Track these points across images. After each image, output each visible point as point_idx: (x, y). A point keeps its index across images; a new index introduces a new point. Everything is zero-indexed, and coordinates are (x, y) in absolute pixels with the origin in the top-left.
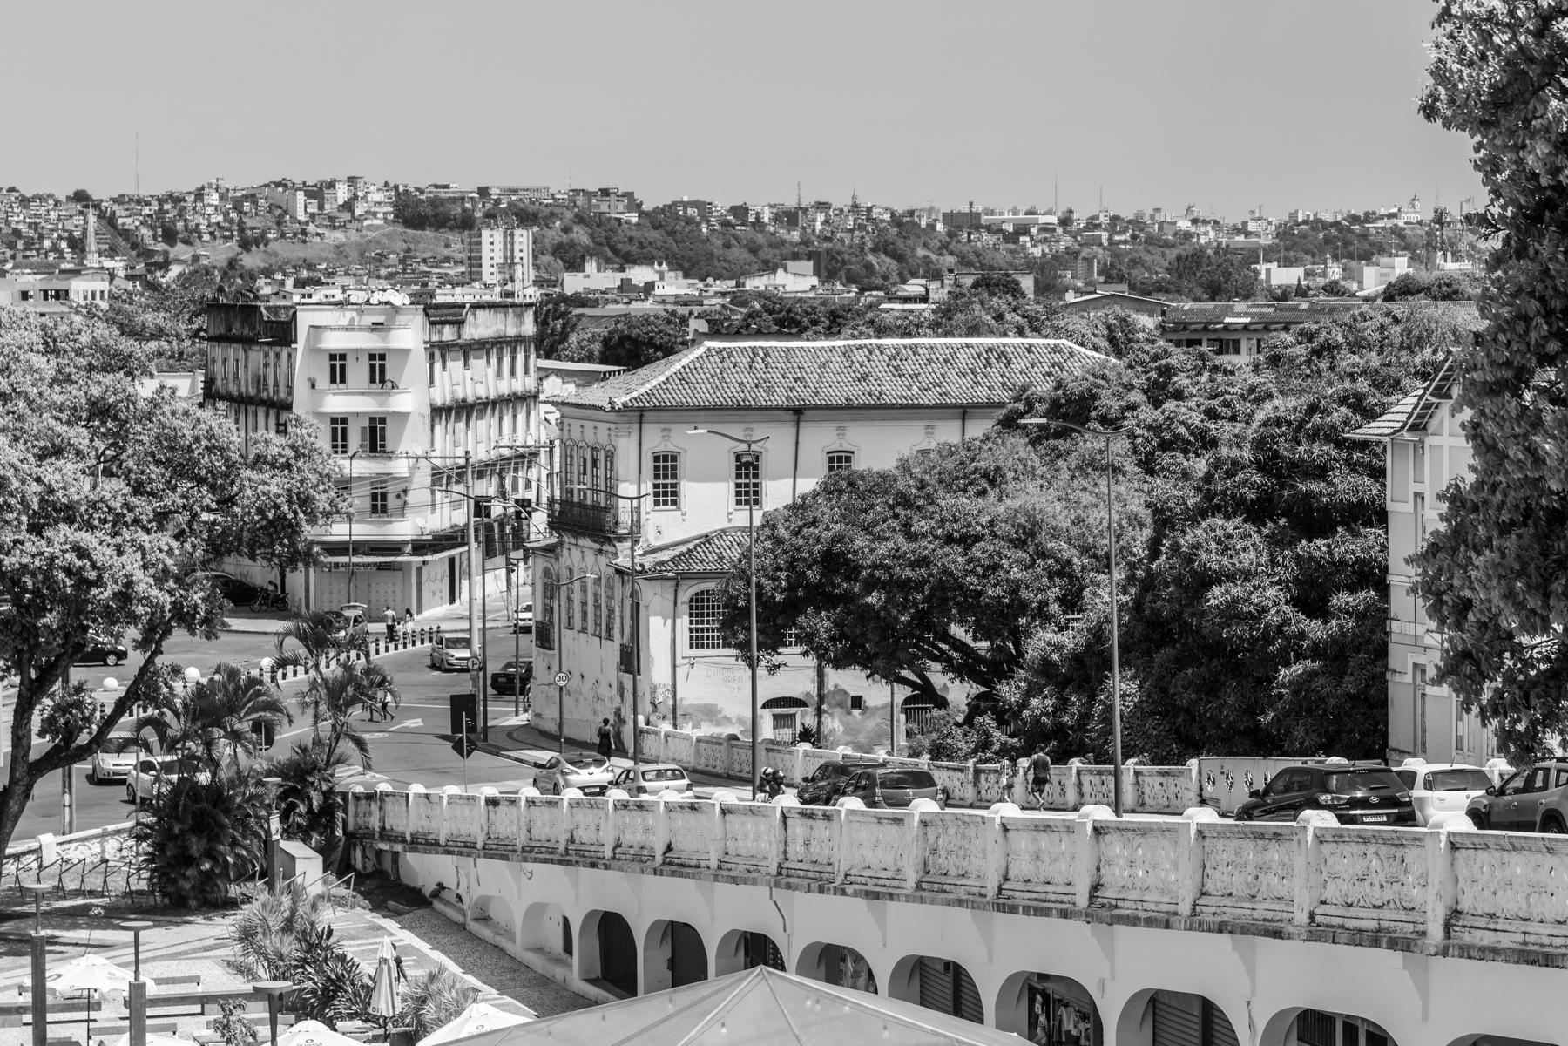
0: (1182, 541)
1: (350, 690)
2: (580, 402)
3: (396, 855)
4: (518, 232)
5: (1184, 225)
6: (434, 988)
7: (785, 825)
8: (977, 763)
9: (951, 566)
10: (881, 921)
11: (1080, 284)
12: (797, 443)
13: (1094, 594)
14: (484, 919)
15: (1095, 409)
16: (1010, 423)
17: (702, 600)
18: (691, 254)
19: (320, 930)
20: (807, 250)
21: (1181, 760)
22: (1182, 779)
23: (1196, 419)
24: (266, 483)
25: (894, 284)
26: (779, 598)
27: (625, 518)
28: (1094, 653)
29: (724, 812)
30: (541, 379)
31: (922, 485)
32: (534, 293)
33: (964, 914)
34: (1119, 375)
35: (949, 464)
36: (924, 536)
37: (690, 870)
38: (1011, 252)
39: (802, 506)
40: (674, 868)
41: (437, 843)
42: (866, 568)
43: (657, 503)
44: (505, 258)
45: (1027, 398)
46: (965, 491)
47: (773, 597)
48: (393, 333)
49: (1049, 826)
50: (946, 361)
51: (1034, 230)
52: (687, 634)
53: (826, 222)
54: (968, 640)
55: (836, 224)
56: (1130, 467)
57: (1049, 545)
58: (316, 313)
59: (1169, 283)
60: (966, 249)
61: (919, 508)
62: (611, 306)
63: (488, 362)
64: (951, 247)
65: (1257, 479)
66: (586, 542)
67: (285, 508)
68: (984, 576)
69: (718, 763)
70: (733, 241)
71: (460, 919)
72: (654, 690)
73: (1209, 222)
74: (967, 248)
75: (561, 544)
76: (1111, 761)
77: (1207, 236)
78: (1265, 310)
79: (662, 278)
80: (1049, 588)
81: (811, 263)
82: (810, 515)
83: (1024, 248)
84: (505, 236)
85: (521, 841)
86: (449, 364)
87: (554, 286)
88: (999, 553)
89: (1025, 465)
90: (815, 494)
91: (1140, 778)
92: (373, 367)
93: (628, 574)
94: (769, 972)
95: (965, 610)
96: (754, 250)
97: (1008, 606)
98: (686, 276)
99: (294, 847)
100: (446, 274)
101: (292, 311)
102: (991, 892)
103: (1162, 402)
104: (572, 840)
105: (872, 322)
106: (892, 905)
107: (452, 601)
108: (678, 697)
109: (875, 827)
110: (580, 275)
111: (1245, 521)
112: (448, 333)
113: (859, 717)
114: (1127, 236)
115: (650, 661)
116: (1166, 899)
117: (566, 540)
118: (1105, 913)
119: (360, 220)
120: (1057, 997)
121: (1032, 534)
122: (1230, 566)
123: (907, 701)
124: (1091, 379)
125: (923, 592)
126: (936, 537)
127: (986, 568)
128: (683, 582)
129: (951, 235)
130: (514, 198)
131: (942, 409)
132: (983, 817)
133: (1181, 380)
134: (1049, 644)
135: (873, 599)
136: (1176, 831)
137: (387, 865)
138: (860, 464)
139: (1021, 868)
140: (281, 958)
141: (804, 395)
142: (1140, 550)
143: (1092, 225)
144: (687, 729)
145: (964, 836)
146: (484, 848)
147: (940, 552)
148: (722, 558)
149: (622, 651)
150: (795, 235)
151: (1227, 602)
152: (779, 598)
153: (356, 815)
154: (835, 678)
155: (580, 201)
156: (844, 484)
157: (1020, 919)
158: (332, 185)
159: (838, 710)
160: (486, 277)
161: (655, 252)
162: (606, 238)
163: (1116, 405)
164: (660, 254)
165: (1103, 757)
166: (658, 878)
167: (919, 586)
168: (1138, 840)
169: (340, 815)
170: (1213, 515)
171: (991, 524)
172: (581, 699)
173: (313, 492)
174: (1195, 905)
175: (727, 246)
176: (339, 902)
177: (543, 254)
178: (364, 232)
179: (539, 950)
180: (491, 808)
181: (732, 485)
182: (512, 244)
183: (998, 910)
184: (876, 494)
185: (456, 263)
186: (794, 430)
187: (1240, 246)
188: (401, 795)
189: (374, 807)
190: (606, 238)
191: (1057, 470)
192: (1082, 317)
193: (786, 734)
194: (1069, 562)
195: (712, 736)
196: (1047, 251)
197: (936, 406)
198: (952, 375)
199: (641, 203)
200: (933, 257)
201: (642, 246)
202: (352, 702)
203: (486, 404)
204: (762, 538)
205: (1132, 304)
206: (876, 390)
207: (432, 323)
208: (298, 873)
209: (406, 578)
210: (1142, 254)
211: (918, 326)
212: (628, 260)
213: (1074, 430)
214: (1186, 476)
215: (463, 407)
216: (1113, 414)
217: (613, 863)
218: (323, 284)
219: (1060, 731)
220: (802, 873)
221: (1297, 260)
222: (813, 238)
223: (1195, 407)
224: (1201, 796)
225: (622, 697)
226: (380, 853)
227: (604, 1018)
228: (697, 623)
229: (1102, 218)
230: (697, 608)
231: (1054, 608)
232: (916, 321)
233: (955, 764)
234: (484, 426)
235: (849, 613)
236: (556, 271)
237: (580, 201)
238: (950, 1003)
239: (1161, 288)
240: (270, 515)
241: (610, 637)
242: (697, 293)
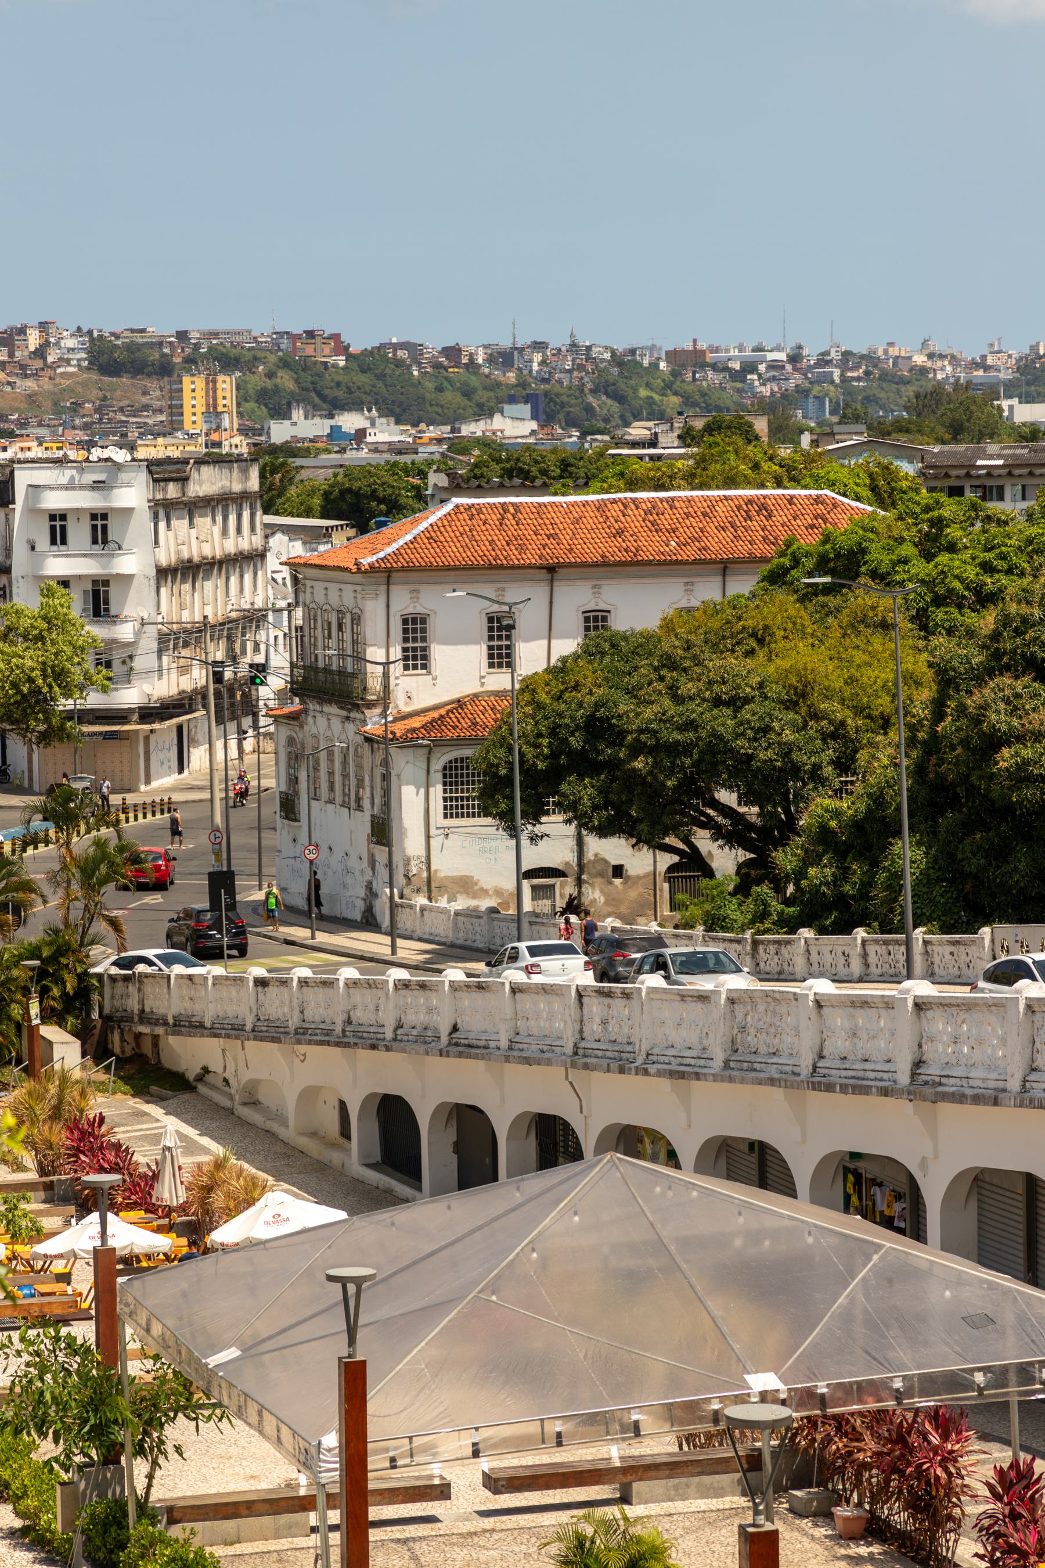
0: (969, 702)
1: (103, 869)
2: (324, 563)
3: (156, 1038)
4: (220, 378)
5: (919, 359)
7: (581, 1003)
9: (721, 729)
12: (551, 603)
13: (873, 756)
14: (253, 1103)
15: (865, 563)
16: (776, 578)
17: (456, 768)
18: (402, 398)
19: (91, 1117)
20: (524, 393)
23: (971, 572)
24: (20, 656)
25: (617, 427)
26: (541, 765)
27: (375, 683)
30: (267, 537)
31: (688, 647)
33: (777, 1094)
34: (889, 527)
35: (715, 624)
36: (691, 698)
37: (478, 1051)
38: (739, 391)
40: (460, 1049)
41: (201, 1026)
42: (631, 733)
43: (406, 667)
44: (208, 405)
45: (794, 553)
46: (733, 651)
47: (535, 764)
48: (116, 491)
49: (866, 1002)
50: (705, 515)
51: (762, 368)
52: (441, 804)
53: (543, 363)
54: (734, 805)
55: (553, 365)
56: (902, 621)
58: (35, 472)
59: (910, 422)
60: (689, 388)
61: (685, 670)
63: (214, 520)
64: (675, 386)
66: (333, 709)
67: (40, 682)
68: (755, 739)
69: (478, 937)
70: (446, 384)
71: (228, 1103)
72: (407, 861)
73: (946, 357)
75: (305, 711)
77: (944, 372)
78: (1018, 451)
79: (373, 425)
80: (823, 750)
81: (528, 406)
82: (571, 679)
83: (752, 386)
84: (207, 384)
85: (294, 1022)
87: (260, 435)
88: (770, 715)
89: (794, 623)
90: (576, 657)
91: (929, 948)
92: (94, 528)
93: (378, 742)
94: (619, 1159)
96: (467, 393)
98: (398, 422)
99: (50, 1032)
100: (146, 424)
101: (8, 471)
102: (805, 1071)
103: (935, 556)
104: (349, 1021)
105: (622, 474)
106: (695, 1084)
108: (433, 868)
109: (678, 1005)
110: (287, 423)
111: (1034, 680)
112: (172, 491)
113: (620, 887)
115: (403, 832)
116: (994, 1076)
117: (311, 707)
118: (928, 1090)
119: (53, 367)
120: (870, 1176)
121: (803, 695)
122: (1019, 727)
123: (671, 869)
124: (861, 532)
125: (691, 756)
126: (704, 700)
127: (757, 731)
128: (435, 750)
129: (675, 374)
130: (214, 342)
132: (795, 994)
133: (954, 532)
134: (827, 811)
135: (638, 764)
136: (1003, 1006)
137: (147, 1048)
138: (621, 623)
139: (838, 1045)
140: (50, 1147)
141: (557, 553)
142: (921, 711)
143: (823, 360)
144: (443, 903)
145: (774, 1013)
146: (253, 1030)
147: (708, 715)
148: (475, 724)
149: (372, 822)
150: (511, 376)
151: (1017, 764)
152: (541, 765)
153: (113, 997)
155: (285, 343)
156: (607, 646)
157: (837, 1097)
158: (22, 331)
159: (598, 881)
160: (187, 426)
162: (313, 383)
164: (369, 399)
166: (444, 1059)
167: (685, 749)
168: (963, 1015)
169: (95, 997)
170: (1001, 674)
171: (761, 685)
174: (1025, 1081)
175: (440, 389)
176: (101, 1088)
177: (246, 400)
178: (58, 380)
179: (314, 1134)
180: (260, 989)
181: (484, 648)
182: (215, 391)
183: (814, 1089)
184: (640, 656)
186: (548, 588)
187: (979, 381)
189: (132, 989)
190: (313, 383)
191: (827, 628)
194: (843, 723)
195: (468, 909)
196: (776, 389)
197: (695, 562)
199: (349, 345)
200: (657, 397)
201: (350, 391)
202: (104, 881)
204: (522, 704)
206: (632, 545)
207: (155, 481)
208: (55, 1058)
209: (134, 747)
211: (671, 477)
212: (333, 406)
213: (843, 586)
214: (970, 634)
215: (188, 568)
216: (883, 569)
217: (395, 1045)
218: (17, 436)
219: (841, 901)
220: (600, 1053)
222: (531, 380)
225: (373, 869)
226: (138, 1036)
227: (449, 1207)
228: (451, 792)
229: (833, 354)
230: (451, 776)
231: (828, 771)
238: (756, 1179)
239: (901, 427)
240: (25, 690)
241: (359, 808)
242: (410, 440)
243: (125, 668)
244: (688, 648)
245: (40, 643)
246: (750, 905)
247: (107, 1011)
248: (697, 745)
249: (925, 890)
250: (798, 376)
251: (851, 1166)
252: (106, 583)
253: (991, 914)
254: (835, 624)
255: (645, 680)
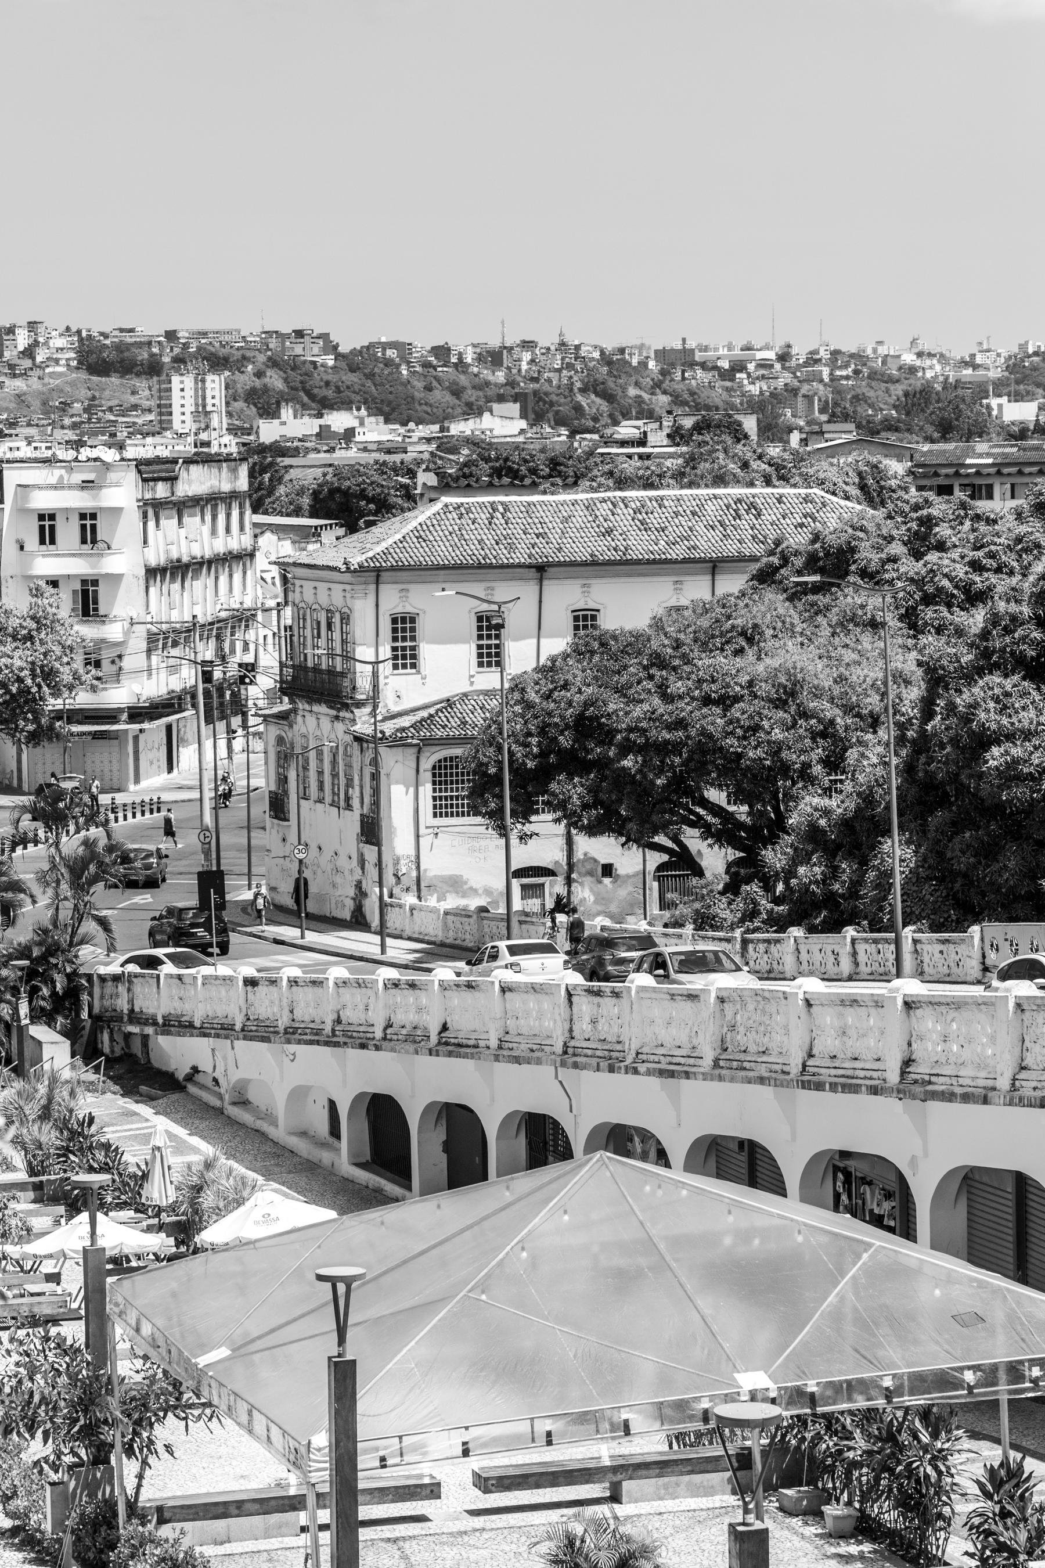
0: (958, 701)
1: (92, 868)
2: (313, 562)
3: (145, 1038)
4: (209, 378)
5: (909, 358)
6: (210, 1175)
8: (745, 933)
9: (711, 728)
10: (675, 1099)
11: (802, 423)
12: (540, 602)
13: (863, 755)
14: (243, 1103)
15: (854, 562)
17: (446, 767)
18: (391, 397)
19: (81, 1117)
21: (960, 926)
22: (963, 946)
23: (961, 571)
25: (605, 426)
26: (530, 764)
28: (863, 817)
29: (503, 990)
30: (256, 536)
31: (678, 645)
32: (230, 444)
33: (766, 1092)
34: (878, 526)
35: (705, 622)
36: (681, 697)
37: (468, 1050)
38: (728, 390)
39: (552, 669)
40: (450, 1048)
42: (621, 732)
43: (395, 667)
44: (197, 405)
46: (722, 650)
47: (524, 764)
48: (104, 491)
49: (855, 1001)
50: (694, 513)
51: (751, 367)
52: (430, 803)
53: (532, 361)
54: (724, 804)
56: (892, 621)
57: (811, 705)
60: (679, 387)
61: (674, 669)
62: (312, 456)
65: (1037, 635)
66: (322, 709)
67: (29, 681)
68: (745, 738)
69: (468, 936)
70: (435, 383)
71: (217, 1103)
72: (397, 862)
73: (934, 355)
74: (681, 386)
75: (295, 711)
76: (891, 927)
77: (932, 370)
78: (1008, 450)
81: (518, 405)
82: (561, 678)
83: (741, 386)
84: (196, 383)
85: (283, 1022)
86: (163, 522)
87: (249, 434)
88: (759, 713)
89: (784, 622)
90: (566, 656)
91: (919, 947)
92: (83, 527)
93: (367, 741)
95: (725, 772)
96: (457, 392)
97: (770, 768)
98: (387, 421)
99: (39, 1031)
100: (134, 423)
102: (795, 1069)
103: (924, 554)
104: (338, 1021)
105: (611, 473)
106: (686, 1085)
107: (170, 769)
110: (276, 422)
111: (1024, 678)
112: (161, 490)
113: (610, 886)
114: (849, 371)
116: (983, 1074)
117: (300, 706)
118: (918, 1089)
120: (859, 1175)
121: (793, 694)
123: (660, 868)
124: (850, 531)
125: (681, 756)
126: (693, 699)
128: (425, 749)
129: (664, 373)
131: (690, 564)
133: (943, 531)
134: (816, 809)
135: (628, 763)
136: (993, 1004)
137: (137, 1048)
138: (608, 622)
140: (40, 1147)
141: (547, 552)
143: (813, 360)
144: (432, 901)
145: (764, 1012)
146: (243, 1030)
148: (465, 723)
149: (362, 821)
150: (500, 376)
151: (1007, 763)
153: (102, 997)
154: (584, 845)
156: (596, 645)
157: (826, 1096)
158: (11, 330)
159: (588, 880)
160: (177, 425)
161: (353, 396)
162: (302, 382)
163: (875, 557)
164: (358, 398)
165: (876, 926)
166: (434, 1058)
167: (676, 747)
168: (953, 1014)
169: (85, 997)
171: (751, 684)
172: (319, 872)
173: (57, 665)
174: (1014, 1079)
175: (429, 388)
176: (90, 1087)
177: (235, 400)
178: (46, 380)
179: (303, 1134)
180: (249, 988)
181: (474, 647)
182: (204, 390)
183: (803, 1088)
184: (629, 655)
185: (144, 411)
186: (537, 588)
188: (151, 976)
189: (122, 989)
190: (302, 382)
192: (832, 464)
193: (534, 905)
194: (832, 722)
197: (685, 561)
198: (700, 528)
201: (338, 390)
202: (93, 880)
203: (201, 564)
204: (512, 702)
205: (880, 449)
206: (621, 545)
207: (144, 480)
208: (45, 1059)
209: (123, 747)
210: (865, 390)
211: (661, 476)
212: (323, 405)
213: (832, 585)
214: (960, 632)
215: (177, 568)
216: (873, 567)
217: (385, 1044)
219: (830, 900)
220: (589, 1052)
221: (1028, 393)
222: (519, 379)
223: (958, 559)
224: (983, 963)
225: (363, 868)
226: (128, 1036)
227: (439, 1207)
228: (440, 791)
230: (440, 775)
231: (817, 769)
232: (658, 471)
233: (721, 934)
234: (200, 586)
235: (603, 778)
236: (251, 419)
237: (273, 343)
239: (890, 426)
240: (14, 690)
241: (349, 807)
242: (400, 439)
243: (114, 668)
244: (678, 647)
245: (28, 644)
246: (740, 904)
247: (96, 1010)
248: (686, 744)
249: (915, 888)
250: (787, 375)
251: (841, 1165)
252: (95, 583)
253: (981, 913)
254: (825, 623)
255: (634, 679)
